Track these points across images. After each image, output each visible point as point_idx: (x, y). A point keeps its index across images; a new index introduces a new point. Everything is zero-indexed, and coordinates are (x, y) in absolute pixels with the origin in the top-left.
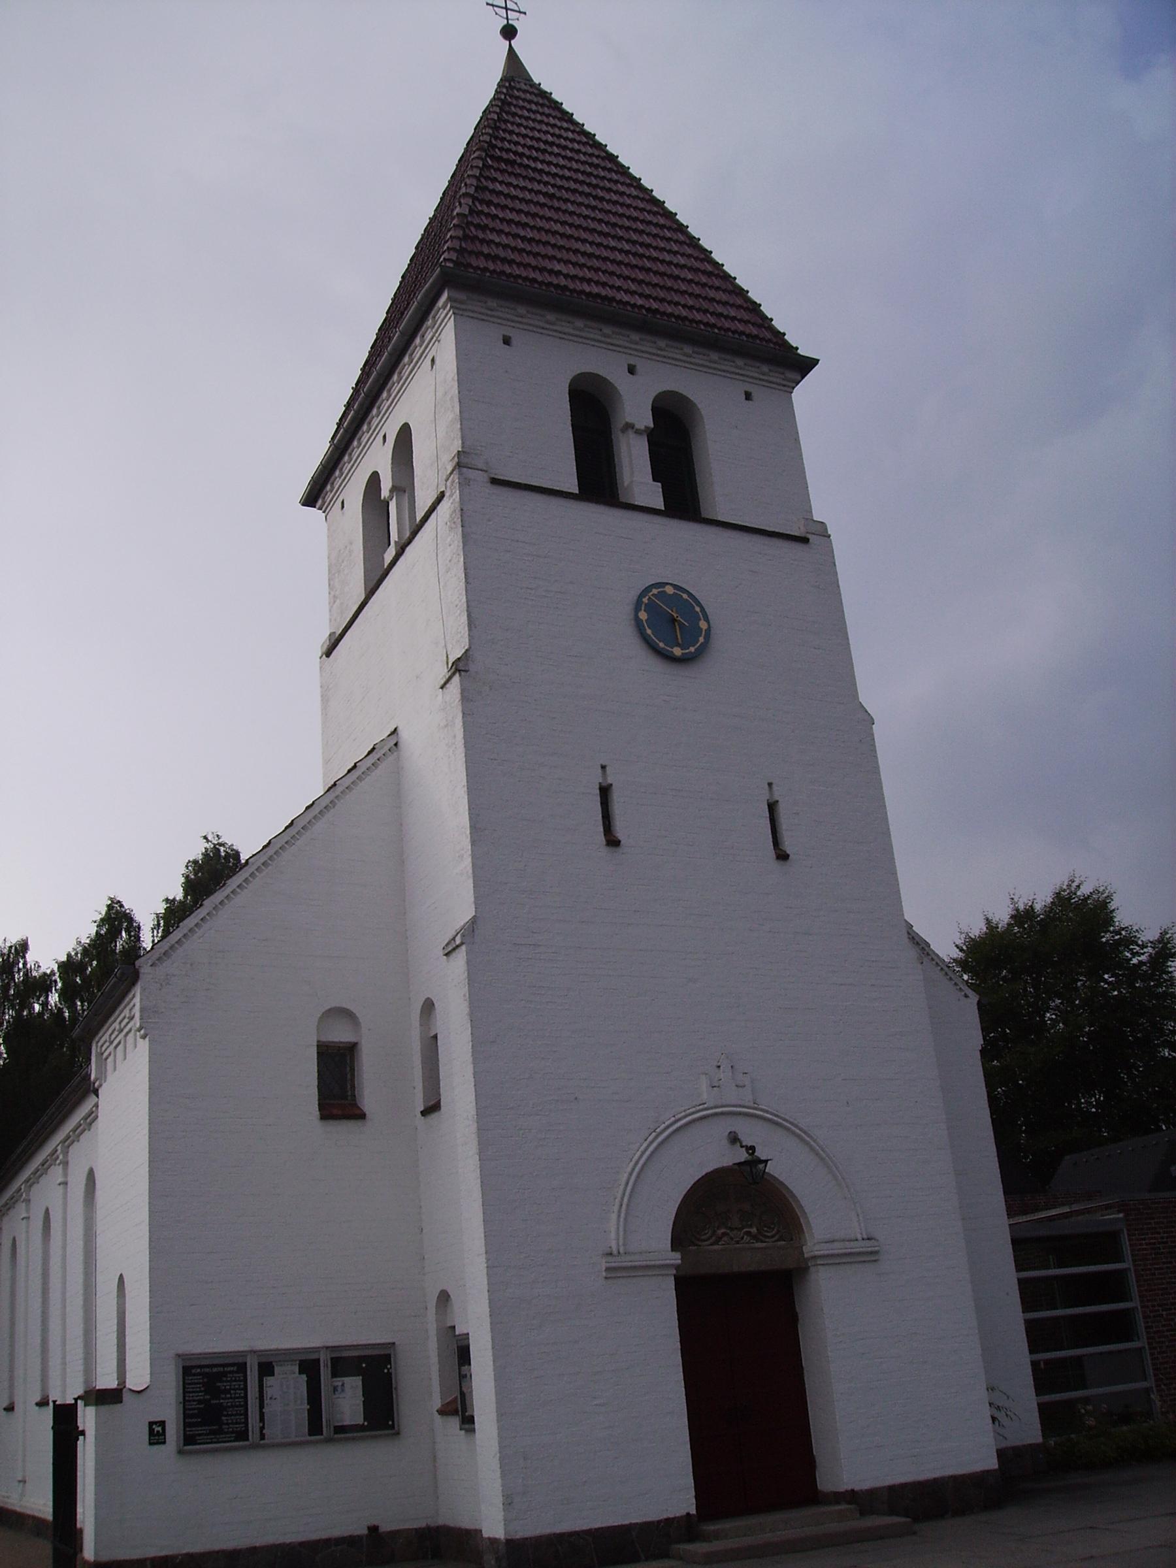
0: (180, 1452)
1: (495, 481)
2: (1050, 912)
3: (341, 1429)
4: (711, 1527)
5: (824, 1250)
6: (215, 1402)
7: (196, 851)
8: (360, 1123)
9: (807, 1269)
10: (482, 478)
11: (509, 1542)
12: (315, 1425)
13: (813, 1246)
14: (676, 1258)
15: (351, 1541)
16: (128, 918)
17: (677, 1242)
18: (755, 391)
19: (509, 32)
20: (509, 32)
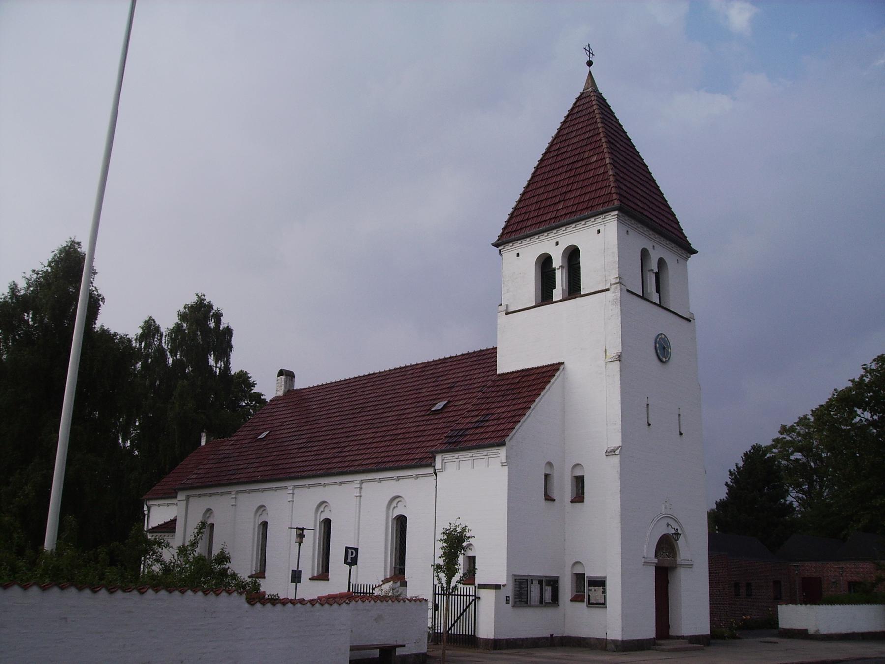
0: (513, 607)
1: (628, 291)
2: (70, 248)
3: (547, 603)
4: (659, 642)
5: (683, 562)
6: (524, 591)
7: (192, 300)
8: (551, 502)
9: (676, 567)
10: (625, 289)
11: (623, 641)
12: (541, 602)
13: (679, 560)
14: (656, 561)
15: (546, 638)
16: (157, 329)
17: (656, 556)
18: (657, 246)
19: (590, 64)
20: (590, 64)
